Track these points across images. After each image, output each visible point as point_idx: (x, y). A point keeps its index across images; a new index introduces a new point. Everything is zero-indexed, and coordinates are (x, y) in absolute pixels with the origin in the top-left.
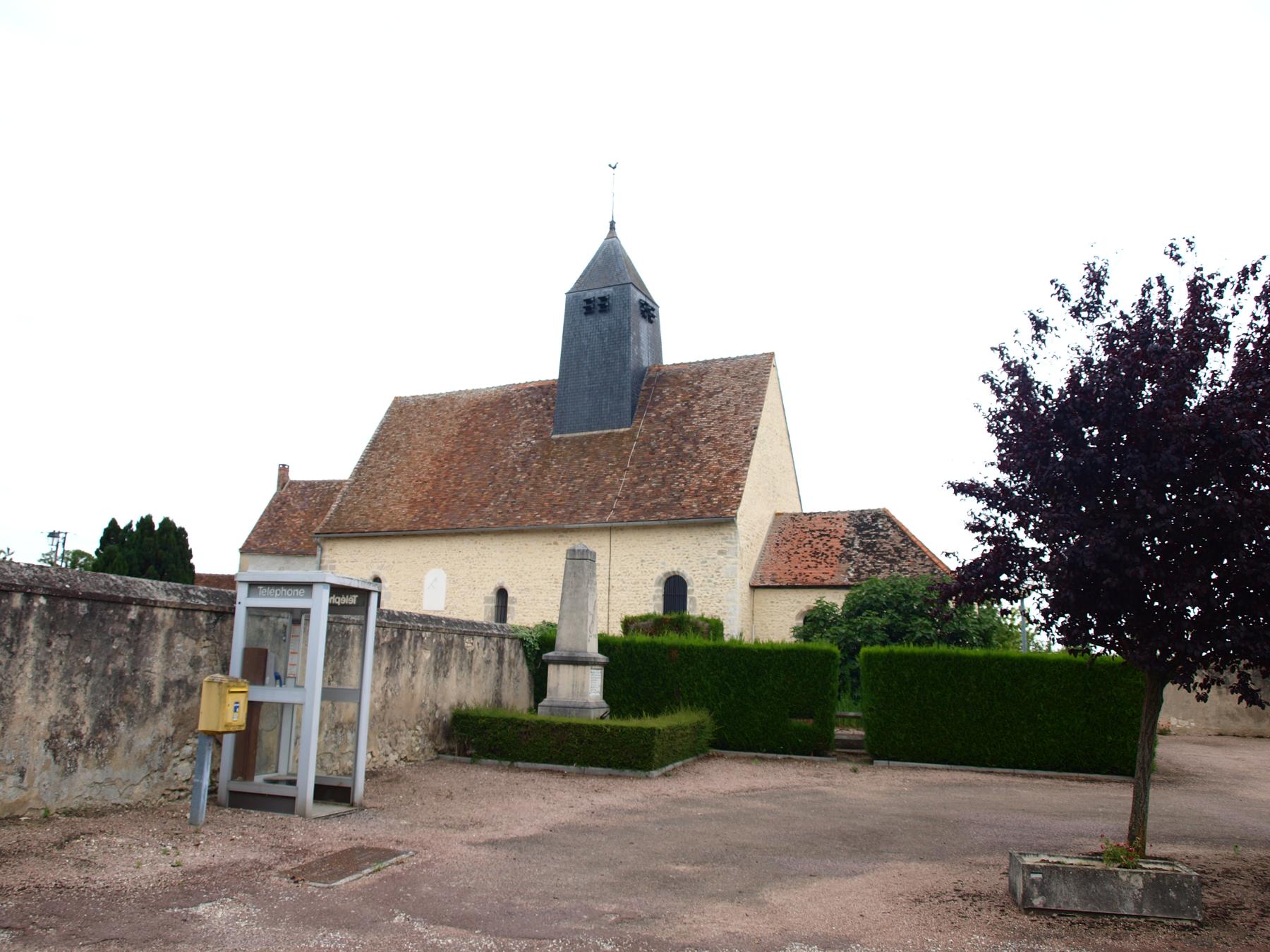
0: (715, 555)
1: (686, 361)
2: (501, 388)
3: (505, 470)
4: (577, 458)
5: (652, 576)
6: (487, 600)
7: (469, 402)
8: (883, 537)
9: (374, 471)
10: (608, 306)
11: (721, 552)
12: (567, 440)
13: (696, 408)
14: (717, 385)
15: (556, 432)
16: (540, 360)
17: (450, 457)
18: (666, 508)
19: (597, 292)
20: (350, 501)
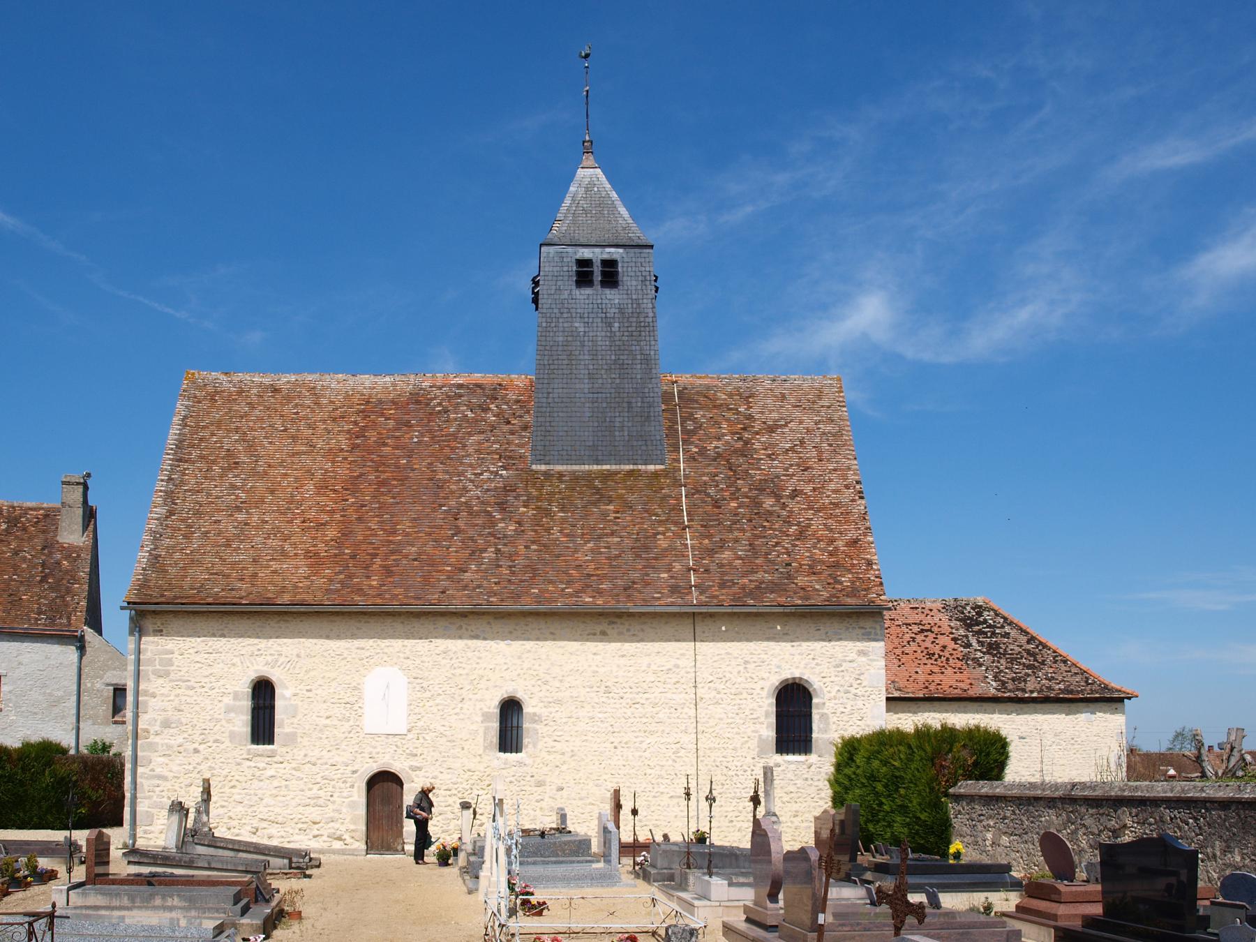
3: (470, 513)
4: (595, 504)
5: (761, 683)
6: (486, 717)
8: (1003, 636)
12: (561, 475)
13: (757, 446)
14: (775, 415)
17: (352, 485)
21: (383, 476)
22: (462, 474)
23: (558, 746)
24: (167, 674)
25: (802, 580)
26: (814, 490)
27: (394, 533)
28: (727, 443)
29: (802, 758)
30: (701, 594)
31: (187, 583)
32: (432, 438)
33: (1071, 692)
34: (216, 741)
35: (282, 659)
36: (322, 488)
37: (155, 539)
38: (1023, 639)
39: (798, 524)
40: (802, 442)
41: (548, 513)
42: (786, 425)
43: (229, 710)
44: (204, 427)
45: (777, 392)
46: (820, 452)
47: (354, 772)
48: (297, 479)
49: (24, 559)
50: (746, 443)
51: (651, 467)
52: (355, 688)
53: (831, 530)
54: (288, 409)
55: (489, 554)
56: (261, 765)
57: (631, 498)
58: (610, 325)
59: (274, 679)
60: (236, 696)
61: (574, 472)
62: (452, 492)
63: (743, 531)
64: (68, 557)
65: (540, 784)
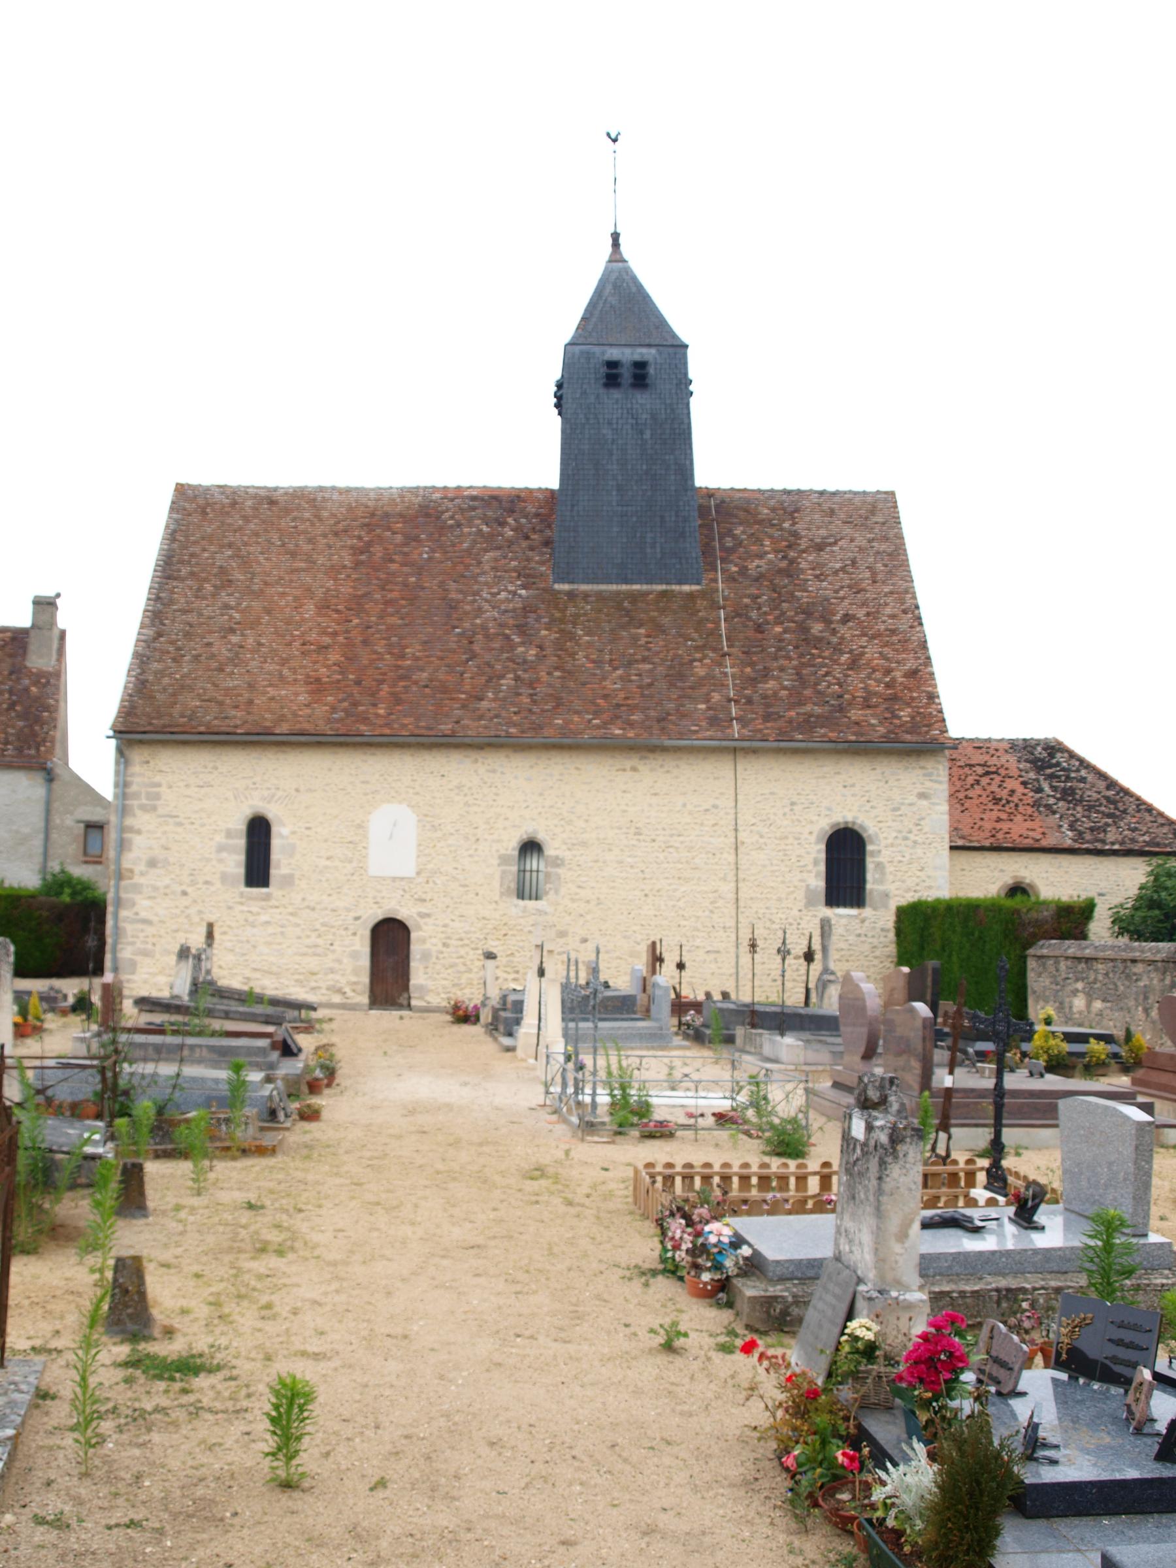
0: (912, 798)
1: (765, 486)
2: (414, 491)
3: (487, 636)
4: (623, 627)
7: (350, 509)
9: (192, 618)
10: (625, 374)
11: (922, 796)
12: (586, 596)
14: (823, 532)
15: (562, 580)
16: (530, 457)
17: (357, 604)
19: (628, 351)
20: (160, 674)
24: (154, 808)
25: (855, 714)
26: (868, 614)
28: (770, 562)
29: (853, 912)
33: (1158, 845)
34: (207, 883)
35: (280, 793)
36: (324, 607)
37: (142, 662)
38: (1101, 785)
39: (851, 652)
40: (854, 562)
41: (572, 637)
42: (835, 543)
44: (195, 543)
45: (825, 507)
46: (874, 574)
47: (357, 918)
48: (296, 599)
50: (792, 562)
51: (686, 588)
52: (360, 826)
55: (507, 682)
56: (255, 909)
62: (466, 613)
64: (36, 683)
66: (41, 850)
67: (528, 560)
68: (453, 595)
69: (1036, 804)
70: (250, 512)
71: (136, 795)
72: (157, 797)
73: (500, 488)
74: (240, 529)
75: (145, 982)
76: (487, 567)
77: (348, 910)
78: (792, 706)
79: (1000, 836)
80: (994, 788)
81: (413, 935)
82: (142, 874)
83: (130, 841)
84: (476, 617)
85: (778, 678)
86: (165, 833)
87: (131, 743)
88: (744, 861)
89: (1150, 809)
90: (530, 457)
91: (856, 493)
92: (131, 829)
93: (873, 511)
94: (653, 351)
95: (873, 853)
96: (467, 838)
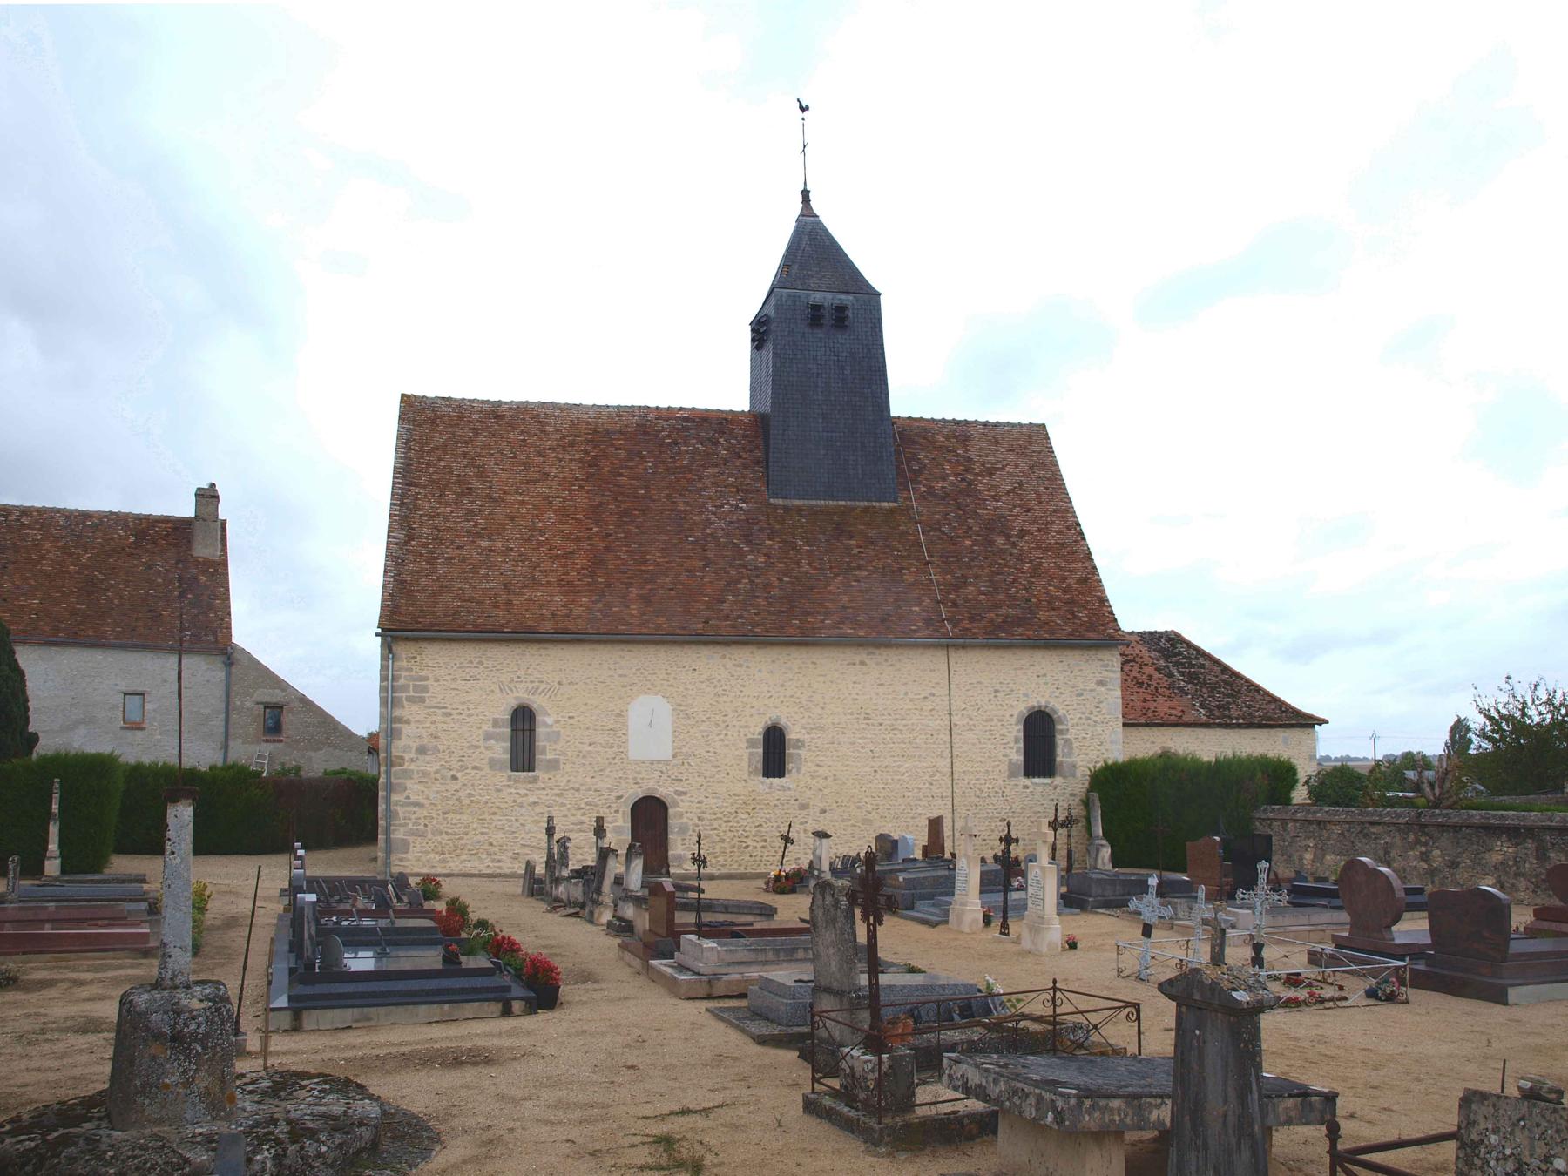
3: (718, 544)
6: (751, 743)
10: (820, 312)
11: (1101, 683)
12: (799, 510)
16: (723, 381)
17: (595, 513)
18: (1020, 622)
19: (829, 296)
21: (623, 506)
22: (703, 506)
23: (821, 770)
24: (423, 700)
25: (1042, 615)
26: (1039, 530)
27: (645, 562)
28: (952, 483)
29: (1047, 781)
30: (955, 626)
31: (439, 610)
32: (667, 469)
33: (1270, 719)
34: (475, 768)
35: (543, 686)
36: (563, 515)
37: (397, 564)
38: (1217, 670)
39: (1031, 562)
40: (1021, 485)
41: (794, 546)
42: (1003, 468)
43: (488, 737)
44: (429, 452)
45: (990, 436)
46: (1039, 495)
47: (619, 798)
48: (535, 507)
49: (159, 573)
50: (970, 483)
51: (885, 504)
52: (619, 715)
53: (1061, 568)
54: (514, 435)
55: (743, 586)
56: (522, 792)
57: (872, 533)
58: (842, 368)
59: (535, 707)
60: (496, 723)
61: (812, 507)
62: (696, 523)
63: (981, 567)
64: (205, 572)
65: (804, 807)
66: (222, 730)
67: (745, 477)
68: (681, 507)
69: (1171, 687)
70: (478, 425)
71: (404, 688)
72: (425, 689)
73: (707, 411)
74: (471, 440)
75: (418, 859)
76: (708, 483)
77: (610, 790)
78: (990, 609)
79: (1150, 714)
80: (1135, 674)
81: (671, 811)
82: (412, 760)
83: (400, 732)
84: (706, 527)
85: (974, 585)
86: (433, 722)
87: (395, 639)
88: (956, 739)
89: (1258, 689)
90: (723, 381)
91: (1013, 425)
92: (399, 720)
93: (1029, 441)
94: (851, 297)
95: (1062, 732)
96: (717, 725)
